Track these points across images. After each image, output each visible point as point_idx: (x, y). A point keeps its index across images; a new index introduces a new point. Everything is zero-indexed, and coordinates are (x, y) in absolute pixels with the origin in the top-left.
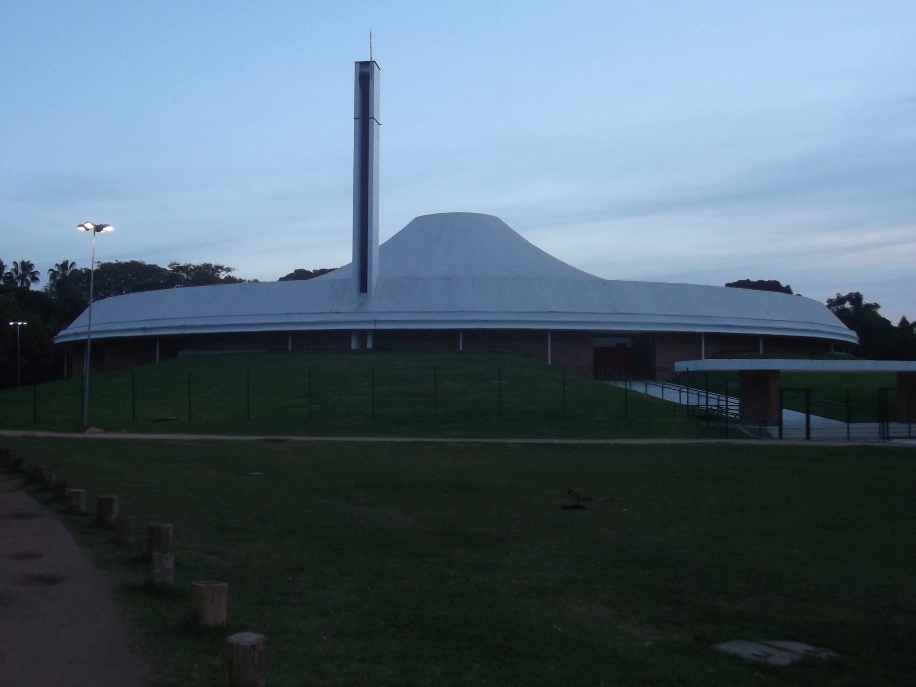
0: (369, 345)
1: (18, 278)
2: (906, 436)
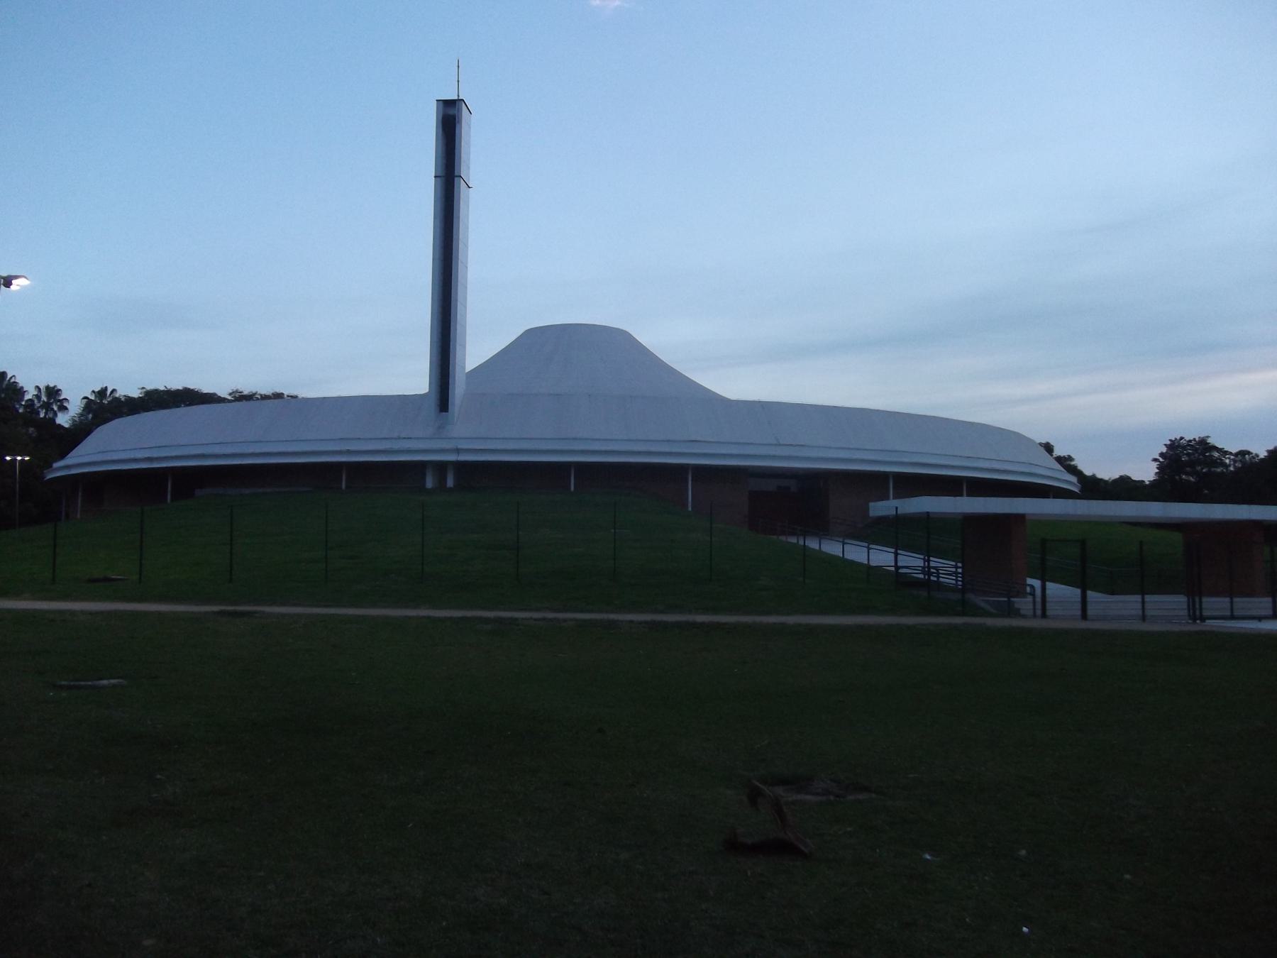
0: (450, 483)
1: (42, 407)
2: (1257, 618)
